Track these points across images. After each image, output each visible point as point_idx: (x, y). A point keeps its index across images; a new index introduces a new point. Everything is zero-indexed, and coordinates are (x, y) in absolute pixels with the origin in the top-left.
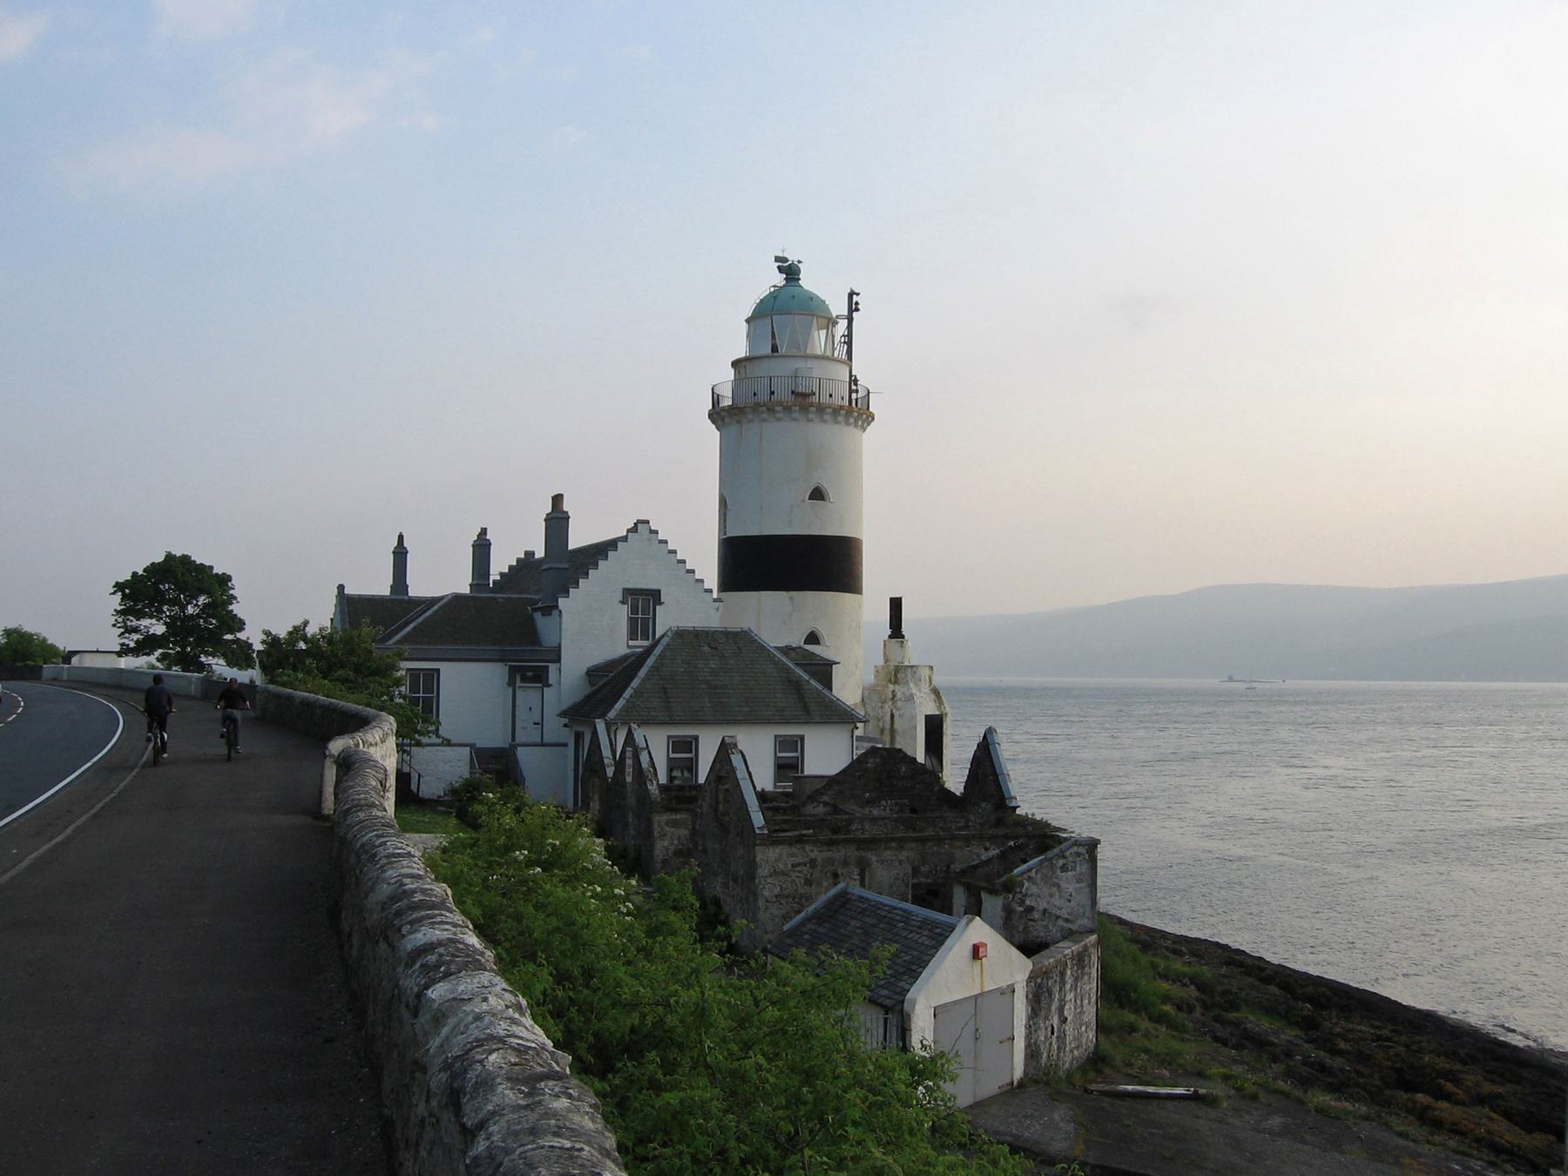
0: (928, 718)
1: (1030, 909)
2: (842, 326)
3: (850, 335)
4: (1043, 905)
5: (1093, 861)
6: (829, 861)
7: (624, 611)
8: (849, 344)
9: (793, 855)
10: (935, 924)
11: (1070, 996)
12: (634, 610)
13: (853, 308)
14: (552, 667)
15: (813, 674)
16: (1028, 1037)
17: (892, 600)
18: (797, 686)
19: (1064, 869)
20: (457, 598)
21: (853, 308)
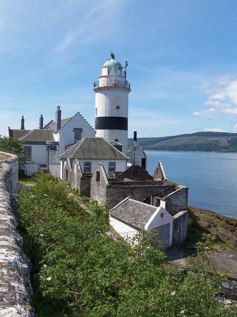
1: (172, 204)
5: (77, 129)
6: (124, 192)
10: (151, 209)
11: (182, 225)
12: (76, 133)
13: (127, 65)
14: (57, 146)
16: (173, 235)
18: (114, 151)
19: (180, 195)
20: (36, 130)
21: (127, 65)
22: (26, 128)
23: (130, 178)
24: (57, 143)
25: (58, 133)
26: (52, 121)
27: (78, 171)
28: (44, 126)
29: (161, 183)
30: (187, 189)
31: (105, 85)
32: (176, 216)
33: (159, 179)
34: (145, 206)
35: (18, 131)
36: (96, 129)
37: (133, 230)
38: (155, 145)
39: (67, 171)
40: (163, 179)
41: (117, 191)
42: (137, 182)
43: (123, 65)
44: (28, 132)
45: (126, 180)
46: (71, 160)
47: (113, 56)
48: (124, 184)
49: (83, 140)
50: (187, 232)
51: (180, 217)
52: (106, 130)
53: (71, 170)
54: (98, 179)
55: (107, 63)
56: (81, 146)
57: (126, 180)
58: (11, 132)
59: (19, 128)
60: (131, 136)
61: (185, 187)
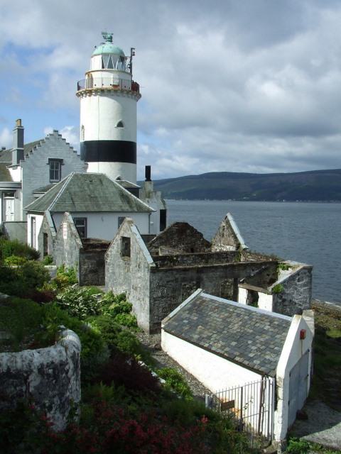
0: (161, 210)
2: (128, 61)
3: (131, 65)
4: (289, 298)
7: (48, 168)
8: (131, 68)
9: (167, 276)
12: (52, 167)
13: (133, 54)
15: (133, 193)
17: (146, 167)
24: (19, 184)
25: (19, 168)
29: (236, 254)
30: (310, 269)
37: (9, 221)
39: (46, 235)
40: (238, 246)
41: (171, 279)
43: (127, 54)
52: (112, 163)
53: (54, 234)
55: (100, 50)
56: (67, 189)
61: (305, 265)
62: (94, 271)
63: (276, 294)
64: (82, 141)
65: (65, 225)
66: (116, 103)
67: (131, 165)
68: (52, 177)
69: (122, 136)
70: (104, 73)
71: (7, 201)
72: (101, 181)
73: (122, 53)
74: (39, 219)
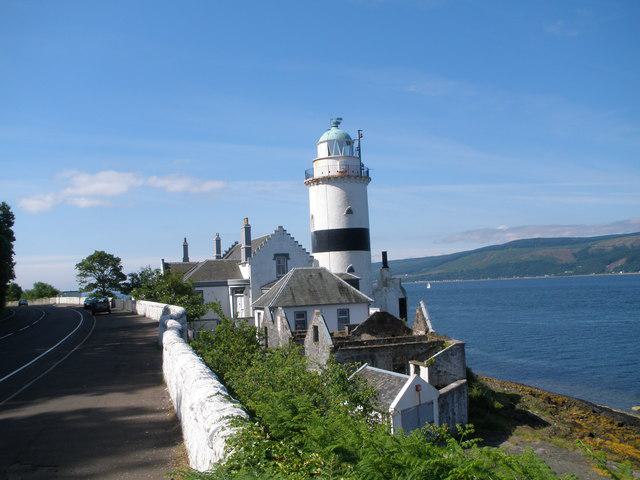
10: (400, 379)
12: (279, 262)
13: (361, 136)
15: (351, 284)
21: (361, 136)
22: (192, 259)
23: (372, 334)
24: (248, 281)
26: (237, 243)
27: (283, 327)
28: (223, 253)
31: (324, 175)
32: (443, 391)
33: (422, 333)
34: (390, 376)
35: (180, 264)
36: (314, 251)
38: (435, 272)
40: (427, 331)
42: (387, 338)
43: (354, 136)
44: (195, 265)
45: (365, 337)
46: (271, 309)
47: (337, 124)
48: (361, 343)
49: (290, 273)
50: (469, 416)
51: (451, 392)
54: (316, 338)
57: (365, 337)
58: (166, 266)
59: (179, 259)
60: (376, 258)
62: (33, 295)
63: (432, 368)
64: (313, 231)
65: (279, 318)
66: (343, 192)
67: (364, 252)
68: (279, 271)
69: (349, 221)
70: (330, 160)
71: (238, 299)
72: (320, 275)
73: (348, 137)
74: (262, 312)
